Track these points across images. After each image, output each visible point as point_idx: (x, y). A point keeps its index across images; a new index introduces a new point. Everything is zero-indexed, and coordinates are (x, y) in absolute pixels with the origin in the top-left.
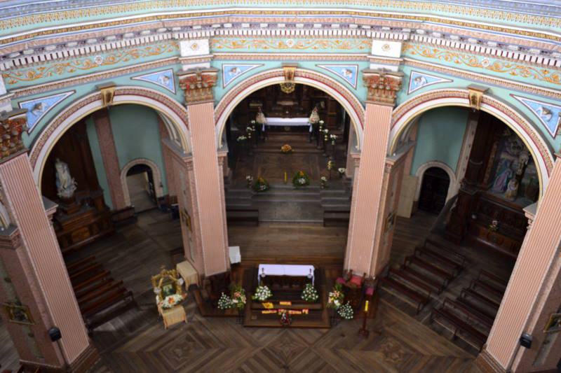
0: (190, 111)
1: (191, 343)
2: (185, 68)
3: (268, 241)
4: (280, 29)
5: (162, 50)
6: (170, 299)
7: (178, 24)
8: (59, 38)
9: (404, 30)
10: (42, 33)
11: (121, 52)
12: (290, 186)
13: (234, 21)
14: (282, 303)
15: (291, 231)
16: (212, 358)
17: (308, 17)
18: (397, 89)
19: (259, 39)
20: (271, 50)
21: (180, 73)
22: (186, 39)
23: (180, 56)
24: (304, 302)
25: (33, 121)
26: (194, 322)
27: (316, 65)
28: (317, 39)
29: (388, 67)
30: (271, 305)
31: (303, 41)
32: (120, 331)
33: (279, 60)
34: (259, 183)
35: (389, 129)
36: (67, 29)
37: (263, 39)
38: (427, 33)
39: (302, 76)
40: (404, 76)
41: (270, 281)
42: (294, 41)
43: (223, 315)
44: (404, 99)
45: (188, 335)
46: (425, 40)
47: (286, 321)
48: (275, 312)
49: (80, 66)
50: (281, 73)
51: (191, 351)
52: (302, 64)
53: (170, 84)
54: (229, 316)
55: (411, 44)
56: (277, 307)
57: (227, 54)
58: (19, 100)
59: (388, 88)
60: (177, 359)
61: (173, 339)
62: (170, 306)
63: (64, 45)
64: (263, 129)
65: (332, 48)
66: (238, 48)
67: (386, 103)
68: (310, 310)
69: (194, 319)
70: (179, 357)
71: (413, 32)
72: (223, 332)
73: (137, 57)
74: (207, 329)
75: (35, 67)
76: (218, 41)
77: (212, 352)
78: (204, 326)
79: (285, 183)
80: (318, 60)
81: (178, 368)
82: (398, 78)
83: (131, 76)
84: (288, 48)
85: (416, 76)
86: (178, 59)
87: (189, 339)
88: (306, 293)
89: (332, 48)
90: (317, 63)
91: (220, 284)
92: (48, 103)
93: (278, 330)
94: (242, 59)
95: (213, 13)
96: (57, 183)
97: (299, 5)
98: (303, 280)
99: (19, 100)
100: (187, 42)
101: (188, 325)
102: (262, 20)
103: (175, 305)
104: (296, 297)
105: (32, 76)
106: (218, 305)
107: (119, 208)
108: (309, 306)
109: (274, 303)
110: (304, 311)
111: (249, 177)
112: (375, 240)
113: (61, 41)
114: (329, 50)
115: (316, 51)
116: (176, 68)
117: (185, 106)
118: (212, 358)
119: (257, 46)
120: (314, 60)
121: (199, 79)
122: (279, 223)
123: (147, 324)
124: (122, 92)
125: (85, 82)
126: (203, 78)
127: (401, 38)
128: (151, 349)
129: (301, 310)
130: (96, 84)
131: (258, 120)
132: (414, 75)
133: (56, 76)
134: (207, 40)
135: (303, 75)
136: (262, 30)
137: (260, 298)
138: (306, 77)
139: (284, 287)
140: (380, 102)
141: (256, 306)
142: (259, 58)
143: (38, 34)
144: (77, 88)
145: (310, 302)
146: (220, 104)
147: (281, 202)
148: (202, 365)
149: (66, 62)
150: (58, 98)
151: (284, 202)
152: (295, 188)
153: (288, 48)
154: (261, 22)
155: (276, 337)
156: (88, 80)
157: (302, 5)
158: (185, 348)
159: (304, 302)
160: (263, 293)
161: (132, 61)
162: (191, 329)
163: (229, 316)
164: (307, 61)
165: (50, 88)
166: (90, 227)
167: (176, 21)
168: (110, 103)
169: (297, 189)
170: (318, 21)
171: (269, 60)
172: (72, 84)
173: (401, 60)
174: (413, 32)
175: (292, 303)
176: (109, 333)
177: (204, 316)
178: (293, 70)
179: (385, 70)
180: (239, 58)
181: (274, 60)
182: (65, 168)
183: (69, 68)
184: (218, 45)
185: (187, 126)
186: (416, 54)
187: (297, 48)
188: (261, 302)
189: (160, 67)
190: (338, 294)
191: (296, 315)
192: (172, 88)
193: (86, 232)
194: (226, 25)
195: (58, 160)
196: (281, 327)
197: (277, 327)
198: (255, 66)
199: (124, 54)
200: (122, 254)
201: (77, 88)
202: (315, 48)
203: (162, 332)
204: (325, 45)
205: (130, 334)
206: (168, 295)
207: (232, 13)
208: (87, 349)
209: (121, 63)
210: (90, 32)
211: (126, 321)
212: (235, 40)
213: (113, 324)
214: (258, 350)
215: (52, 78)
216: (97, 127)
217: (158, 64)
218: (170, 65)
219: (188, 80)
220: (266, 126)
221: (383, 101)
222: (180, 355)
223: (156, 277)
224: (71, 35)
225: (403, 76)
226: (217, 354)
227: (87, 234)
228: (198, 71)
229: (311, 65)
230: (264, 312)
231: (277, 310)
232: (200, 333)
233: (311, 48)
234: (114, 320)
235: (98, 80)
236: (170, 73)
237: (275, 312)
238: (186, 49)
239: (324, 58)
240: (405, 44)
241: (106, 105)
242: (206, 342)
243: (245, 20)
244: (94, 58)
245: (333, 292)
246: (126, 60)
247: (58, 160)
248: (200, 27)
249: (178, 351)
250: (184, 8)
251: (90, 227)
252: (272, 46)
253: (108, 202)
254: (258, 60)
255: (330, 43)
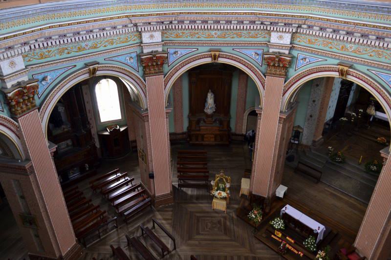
0: (267, 79)
1: (219, 226)
2: (271, 50)
3: (316, 196)
4: (342, 35)
5: (259, 36)
6: (220, 193)
7: (268, 20)
8: (193, 17)
9: (293, 25)
10: (182, 13)
11: (230, 32)
12: (363, 168)
13: (309, 23)
14: (287, 238)
15: (340, 199)
16: (223, 240)
17: (365, 29)
18: (288, 66)
19: (327, 40)
20: (334, 50)
21: (268, 53)
22: (275, 32)
23: (269, 42)
24: (303, 247)
25: (172, 59)
26: (229, 215)
27: (368, 70)
28: (374, 49)
29: (281, 51)
30: (280, 235)
31: (361, 48)
32: (192, 196)
33: (338, 59)
34: (336, 154)
35: (282, 95)
36: (196, 13)
37: (330, 41)
38: (310, 27)
39: (353, 76)
40: (293, 57)
41: (287, 218)
42: (354, 47)
43: (248, 222)
44: (293, 73)
45: (221, 220)
46: (308, 33)
47: (281, 250)
48: (280, 241)
49: (204, 36)
50: (337, 69)
51: (216, 229)
52: (356, 66)
53: (259, 59)
54: (250, 225)
55: (298, 35)
56: (283, 238)
57: (302, 47)
58: (169, 47)
59: (281, 65)
60: (205, 228)
61: (212, 217)
62: (218, 197)
63: (195, 22)
64: (371, 119)
65: (386, 58)
66: (311, 44)
67: (280, 76)
68: (304, 255)
69: (231, 214)
70: (207, 228)
71: (299, 27)
72: (240, 231)
73: (241, 37)
74: (233, 223)
75: (180, 32)
76: (299, 37)
77: (224, 237)
78: (233, 221)
79: (360, 164)
80: (370, 66)
81: (203, 233)
82: (289, 59)
83: (234, 48)
84: (348, 51)
85: (302, 57)
86: (268, 44)
87: (219, 222)
88: (308, 242)
89: (386, 58)
90: (369, 68)
91: (255, 200)
92: (182, 52)
93: (275, 253)
94: (312, 53)
95: (292, 16)
96: (206, 104)
97: (359, 18)
98: (310, 231)
99: (169, 47)
100: (276, 33)
101: (225, 215)
102: (329, 27)
103: (221, 198)
104: (299, 241)
105: (177, 36)
106: (249, 215)
107: (238, 132)
108: (305, 251)
109: (283, 235)
110: (300, 253)
111: (330, 148)
112: (383, 234)
113: (205, 19)
114: (383, 59)
115: (371, 58)
116: (266, 49)
117: (265, 76)
118: (223, 240)
119: (325, 45)
120: (367, 66)
121: (277, 60)
122: (335, 189)
123: (206, 201)
124: (225, 56)
125: (204, 45)
126: (280, 60)
127: (291, 31)
128: (198, 215)
129: (298, 251)
130: (211, 48)
131: (368, 111)
132: (301, 56)
133: (189, 38)
134: (290, 35)
135: (354, 74)
136: (328, 33)
137: (274, 226)
138: (356, 77)
139: (293, 226)
140: (274, 75)
141: (271, 229)
142: (324, 54)
143: (180, 13)
144: (199, 48)
145: (308, 249)
146: (289, 81)
147: (348, 176)
148: (214, 240)
149: (196, 32)
150: (188, 51)
151: (350, 178)
152: (365, 170)
153: (348, 51)
154: (328, 28)
155: (268, 256)
156: (207, 44)
157: (362, 19)
158: (214, 226)
159: (303, 247)
160: (278, 223)
161: (236, 39)
162: (225, 218)
163: (250, 225)
164: (361, 64)
165: (184, 44)
166: (216, 136)
167: (267, 18)
168: (216, 61)
169: (367, 173)
170: (373, 33)
171: (332, 58)
172: (197, 45)
173: (291, 46)
174: (299, 27)
175: (295, 243)
176: (186, 194)
177: (237, 216)
178: (346, 69)
179: (279, 53)
180: (310, 51)
181: (334, 58)
182: (212, 96)
183: (197, 35)
184: (298, 39)
185: (264, 87)
186: (301, 41)
187: (355, 53)
188: (274, 229)
189: (254, 46)
190: (324, 255)
191: (293, 252)
192: (260, 61)
193: (212, 138)
194: (303, 26)
195: (210, 91)
196: (277, 253)
197: (275, 251)
198: (320, 60)
199: (232, 34)
200: (223, 158)
201: (199, 48)
202: (371, 55)
203: (207, 210)
204: (379, 54)
205: (195, 201)
206: (220, 190)
207: (307, 18)
208: (168, 195)
209: (229, 39)
210: (210, 17)
211: (198, 193)
212: (310, 37)
213: (191, 191)
214: (251, 255)
215: (187, 39)
216: (239, 79)
217: (253, 45)
218: (262, 46)
219: (269, 58)
220: (375, 118)
221: (278, 75)
222: (208, 227)
223: (218, 176)
224: (198, 17)
225: (292, 57)
226: (226, 240)
227: (213, 140)
228: (278, 54)
229: (364, 69)
230: (272, 236)
231: (282, 240)
232: (228, 223)
233: (367, 55)
234: (193, 189)
235: (212, 46)
236: (260, 52)
237: (280, 241)
238: (274, 38)
239: (376, 66)
240: (294, 35)
241: (213, 61)
242: (226, 230)
243: (316, 24)
244: (213, 33)
245: (321, 251)
246: (233, 38)
247: (210, 91)
248: (283, 24)
249: (209, 225)
250: (274, 10)
251: (216, 136)
252: (336, 48)
253: (233, 125)
254: (323, 56)
255: (385, 54)
